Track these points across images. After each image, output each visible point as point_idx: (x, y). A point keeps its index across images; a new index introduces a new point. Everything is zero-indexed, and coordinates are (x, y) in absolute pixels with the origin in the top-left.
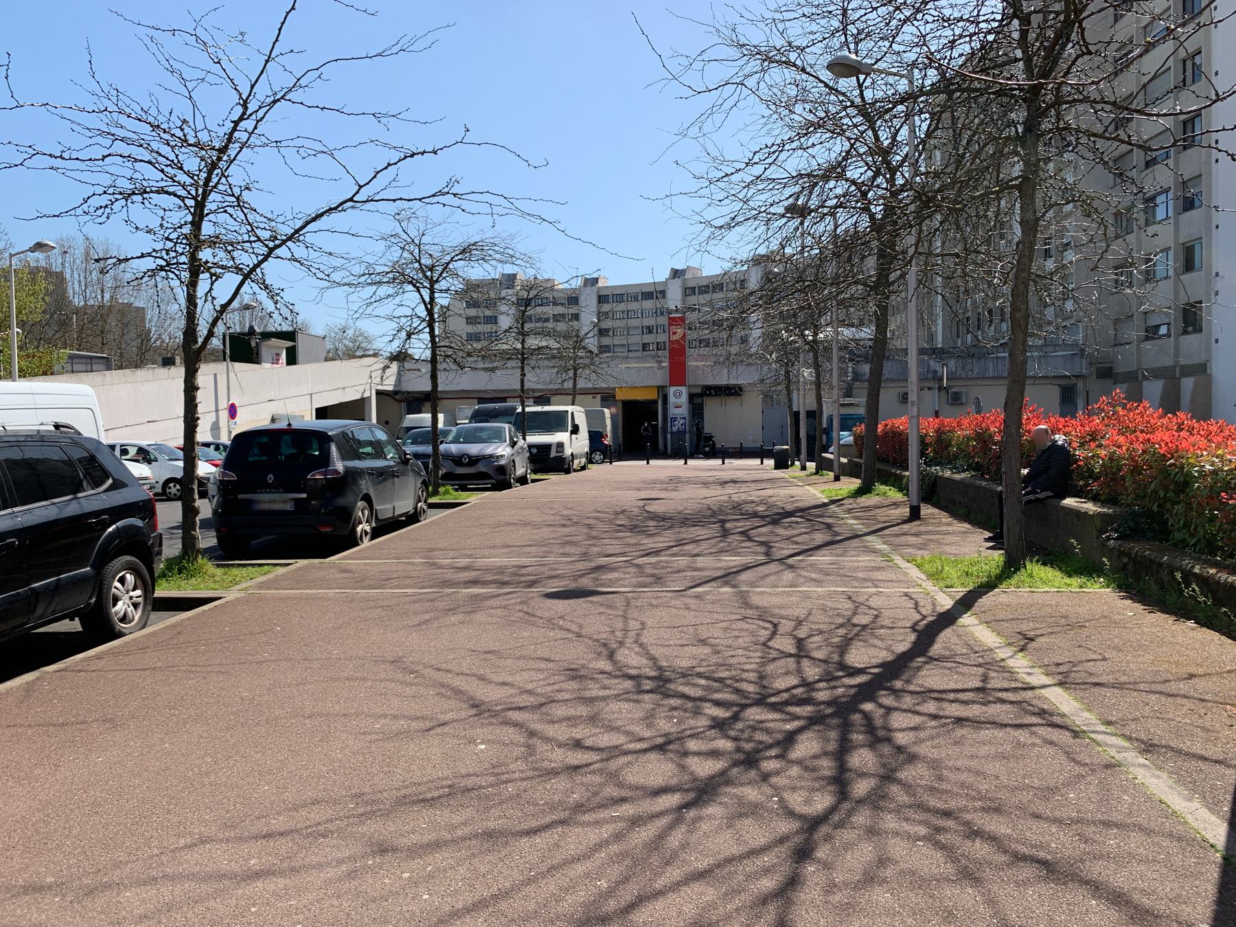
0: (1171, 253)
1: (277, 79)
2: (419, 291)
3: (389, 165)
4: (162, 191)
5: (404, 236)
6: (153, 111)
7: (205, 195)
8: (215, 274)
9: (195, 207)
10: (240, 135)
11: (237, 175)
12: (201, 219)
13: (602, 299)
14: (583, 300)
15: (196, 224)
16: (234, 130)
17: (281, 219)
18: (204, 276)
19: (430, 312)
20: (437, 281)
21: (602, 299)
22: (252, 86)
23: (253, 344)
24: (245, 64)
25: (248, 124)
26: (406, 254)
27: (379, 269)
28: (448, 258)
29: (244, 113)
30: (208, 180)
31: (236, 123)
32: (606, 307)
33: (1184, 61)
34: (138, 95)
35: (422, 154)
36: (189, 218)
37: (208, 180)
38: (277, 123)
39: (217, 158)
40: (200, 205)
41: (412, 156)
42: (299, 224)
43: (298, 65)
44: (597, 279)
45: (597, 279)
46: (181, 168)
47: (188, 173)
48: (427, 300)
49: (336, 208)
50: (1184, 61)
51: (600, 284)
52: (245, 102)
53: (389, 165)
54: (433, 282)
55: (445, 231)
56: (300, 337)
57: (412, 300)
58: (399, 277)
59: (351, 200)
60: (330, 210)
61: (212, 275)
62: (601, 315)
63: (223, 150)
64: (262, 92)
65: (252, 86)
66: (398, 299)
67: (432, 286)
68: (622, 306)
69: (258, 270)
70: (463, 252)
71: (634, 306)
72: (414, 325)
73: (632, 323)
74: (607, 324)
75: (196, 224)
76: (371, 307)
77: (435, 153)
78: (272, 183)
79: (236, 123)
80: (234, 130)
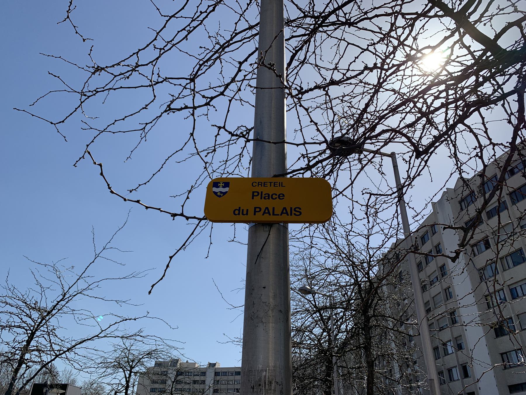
0: (457, 368)
1: (81, 285)
2: (124, 372)
3: (116, 323)
4: (19, 327)
5: (124, 346)
6: (25, 297)
7: (36, 330)
8: (28, 366)
9: (31, 334)
10: (58, 307)
11: (53, 322)
12: (32, 339)
13: (217, 374)
14: (208, 374)
15: (29, 342)
16: (57, 304)
17: (67, 341)
18: (24, 366)
19: (128, 382)
20: (134, 367)
21: (217, 374)
22: (70, 288)
23: (44, 391)
24: (69, 279)
25: (63, 303)
26: (123, 354)
27: (109, 360)
28: (141, 357)
29: (63, 298)
30: (41, 322)
31: (59, 302)
32: (218, 378)
33: (445, 290)
34: (21, 291)
35: (130, 319)
36: (27, 338)
37: (41, 322)
38: (77, 303)
39: (47, 314)
40: (33, 334)
41: (126, 320)
42: (73, 343)
43: (90, 281)
44: (215, 364)
45: (215, 364)
46: (30, 317)
47: (32, 320)
48: (127, 376)
49: (90, 339)
50: (445, 290)
51: (216, 367)
52: (65, 294)
53: (116, 323)
54: (132, 368)
55: (139, 348)
56: (69, 388)
57: (120, 375)
58: (118, 365)
59: (97, 336)
60: (88, 339)
61: (27, 366)
62: (216, 382)
63: (49, 313)
64: (71, 291)
65: (70, 288)
66: (113, 376)
67: (131, 370)
68: (225, 378)
69: (50, 364)
70: (148, 354)
71: (231, 378)
72: (119, 389)
73: (230, 387)
74: (218, 387)
75: (29, 342)
76: (101, 379)
77: (135, 320)
78: (66, 327)
79: (59, 302)
80: (57, 304)
